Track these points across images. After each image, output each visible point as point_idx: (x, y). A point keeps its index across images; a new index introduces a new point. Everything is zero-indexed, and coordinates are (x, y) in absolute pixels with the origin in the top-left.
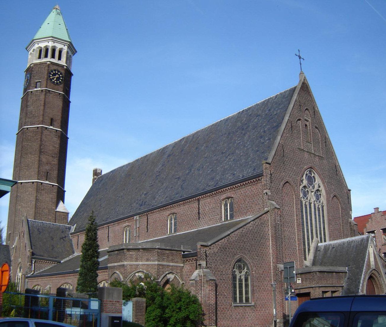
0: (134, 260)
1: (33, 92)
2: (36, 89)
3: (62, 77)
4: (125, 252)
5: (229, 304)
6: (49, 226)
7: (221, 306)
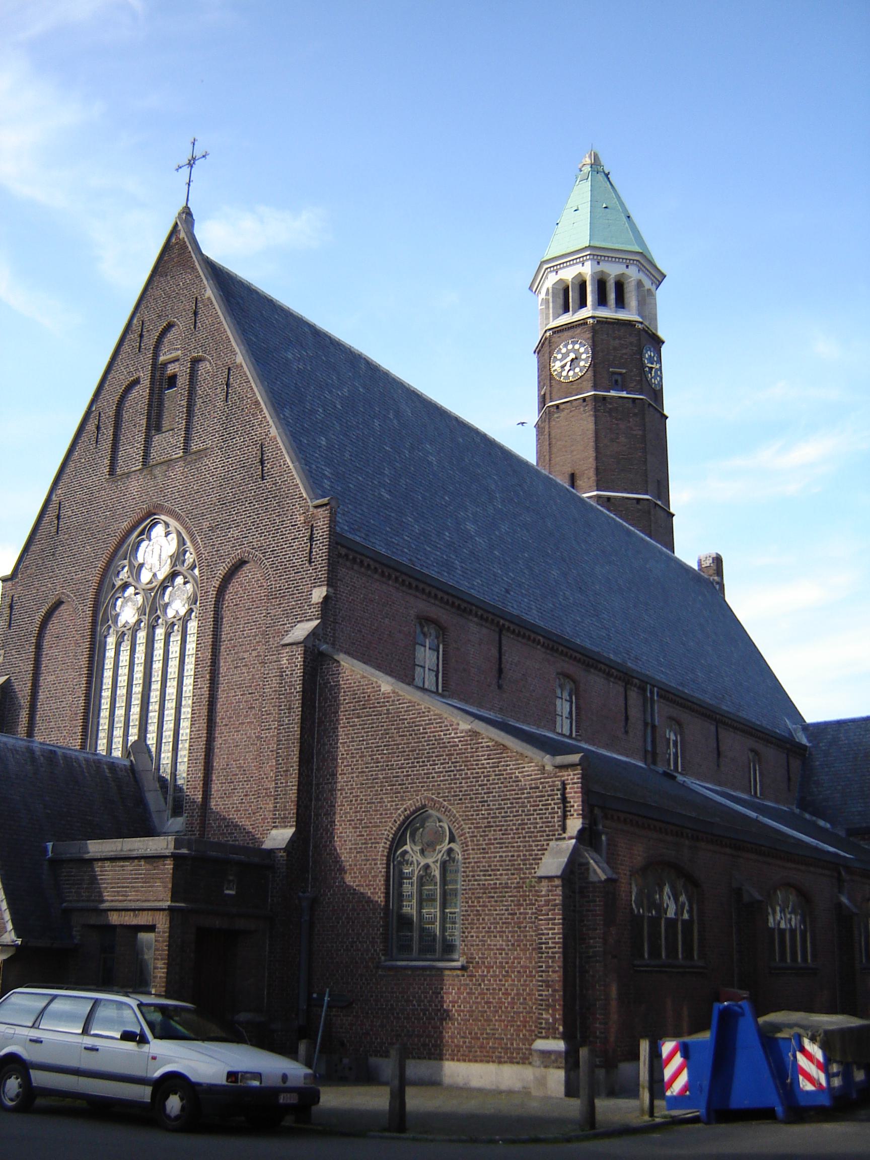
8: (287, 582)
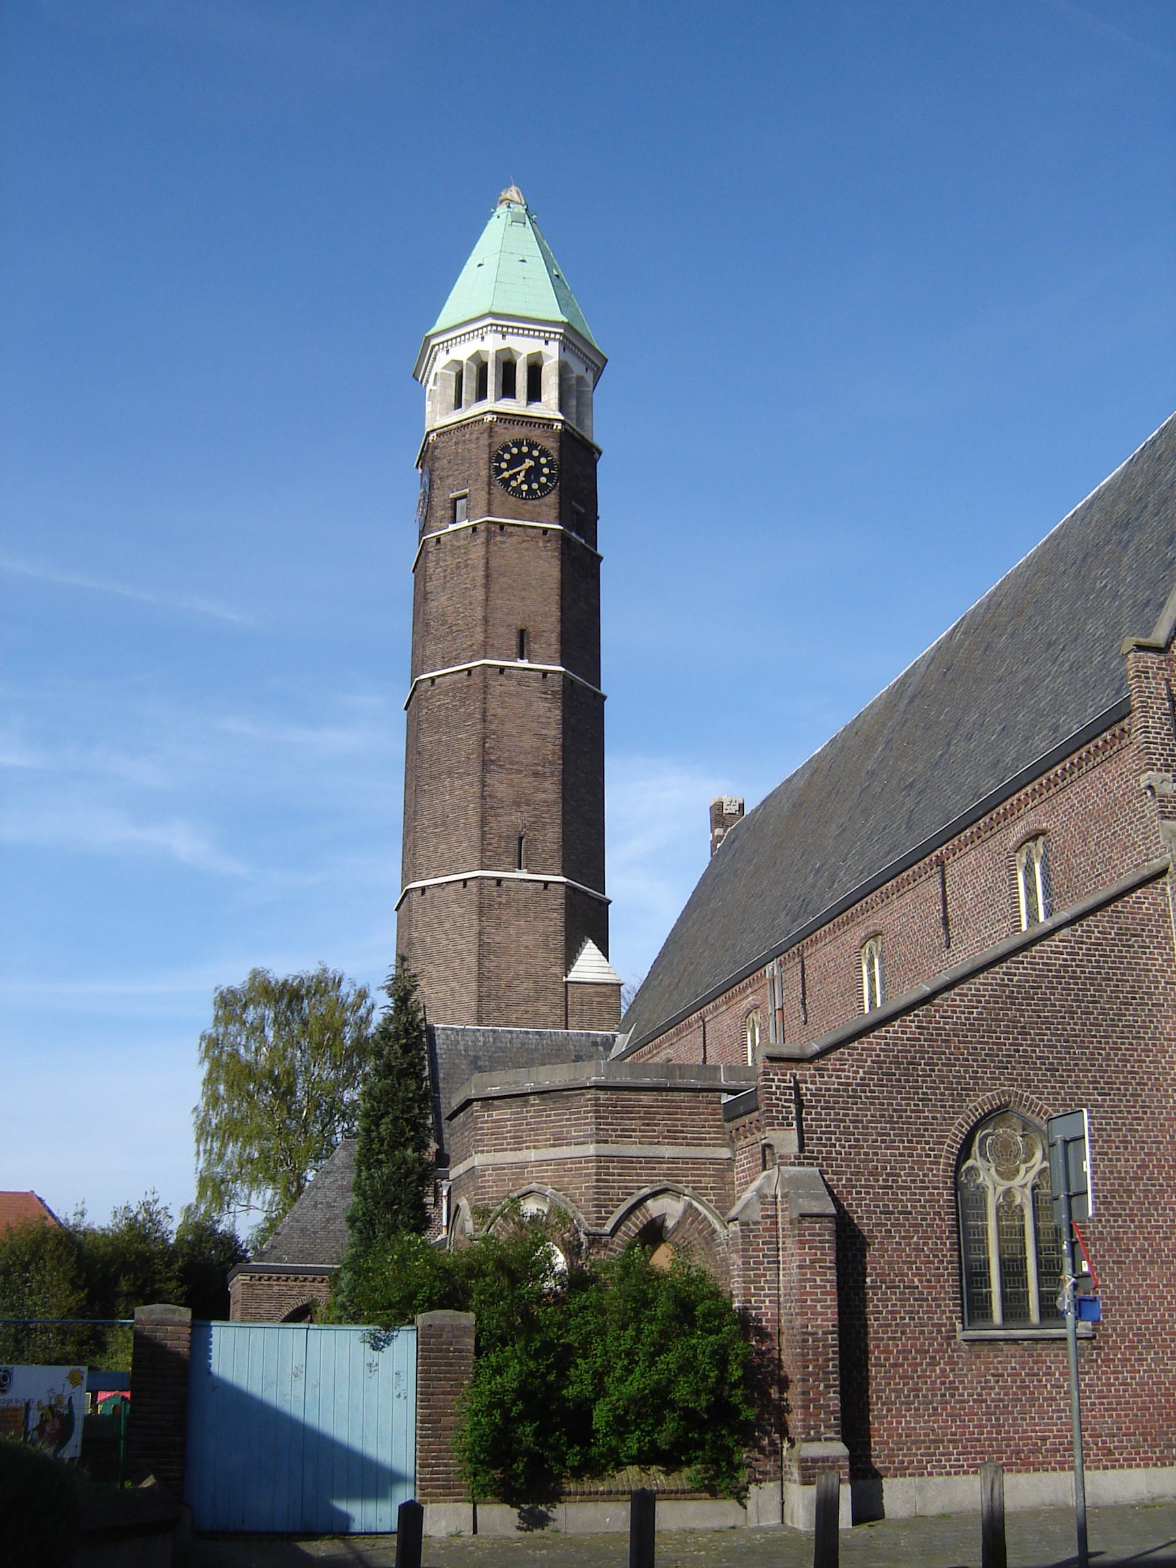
0: (508, 1144)
1: (443, 539)
2: (452, 527)
3: (549, 465)
4: (477, 1111)
5: (939, 1332)
6: (523, 1044)
7: (889, 1338)
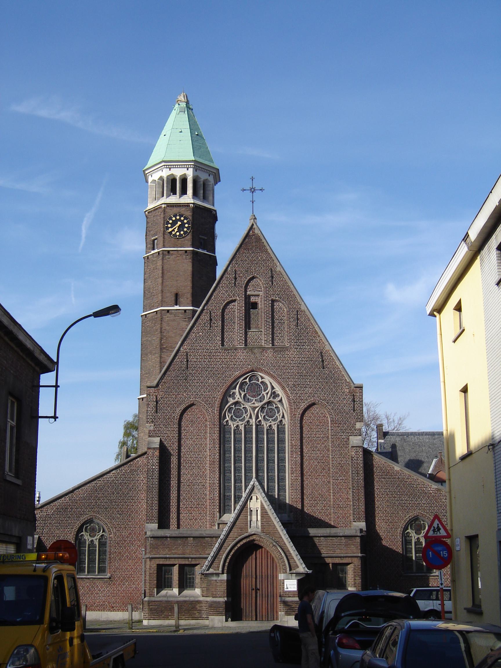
2: (153, 252)
8: (342, 417)
